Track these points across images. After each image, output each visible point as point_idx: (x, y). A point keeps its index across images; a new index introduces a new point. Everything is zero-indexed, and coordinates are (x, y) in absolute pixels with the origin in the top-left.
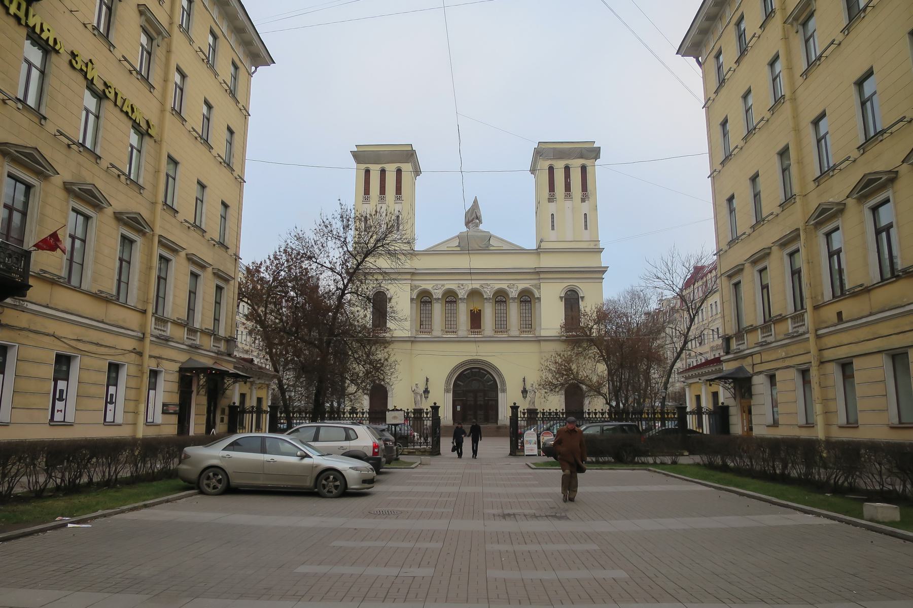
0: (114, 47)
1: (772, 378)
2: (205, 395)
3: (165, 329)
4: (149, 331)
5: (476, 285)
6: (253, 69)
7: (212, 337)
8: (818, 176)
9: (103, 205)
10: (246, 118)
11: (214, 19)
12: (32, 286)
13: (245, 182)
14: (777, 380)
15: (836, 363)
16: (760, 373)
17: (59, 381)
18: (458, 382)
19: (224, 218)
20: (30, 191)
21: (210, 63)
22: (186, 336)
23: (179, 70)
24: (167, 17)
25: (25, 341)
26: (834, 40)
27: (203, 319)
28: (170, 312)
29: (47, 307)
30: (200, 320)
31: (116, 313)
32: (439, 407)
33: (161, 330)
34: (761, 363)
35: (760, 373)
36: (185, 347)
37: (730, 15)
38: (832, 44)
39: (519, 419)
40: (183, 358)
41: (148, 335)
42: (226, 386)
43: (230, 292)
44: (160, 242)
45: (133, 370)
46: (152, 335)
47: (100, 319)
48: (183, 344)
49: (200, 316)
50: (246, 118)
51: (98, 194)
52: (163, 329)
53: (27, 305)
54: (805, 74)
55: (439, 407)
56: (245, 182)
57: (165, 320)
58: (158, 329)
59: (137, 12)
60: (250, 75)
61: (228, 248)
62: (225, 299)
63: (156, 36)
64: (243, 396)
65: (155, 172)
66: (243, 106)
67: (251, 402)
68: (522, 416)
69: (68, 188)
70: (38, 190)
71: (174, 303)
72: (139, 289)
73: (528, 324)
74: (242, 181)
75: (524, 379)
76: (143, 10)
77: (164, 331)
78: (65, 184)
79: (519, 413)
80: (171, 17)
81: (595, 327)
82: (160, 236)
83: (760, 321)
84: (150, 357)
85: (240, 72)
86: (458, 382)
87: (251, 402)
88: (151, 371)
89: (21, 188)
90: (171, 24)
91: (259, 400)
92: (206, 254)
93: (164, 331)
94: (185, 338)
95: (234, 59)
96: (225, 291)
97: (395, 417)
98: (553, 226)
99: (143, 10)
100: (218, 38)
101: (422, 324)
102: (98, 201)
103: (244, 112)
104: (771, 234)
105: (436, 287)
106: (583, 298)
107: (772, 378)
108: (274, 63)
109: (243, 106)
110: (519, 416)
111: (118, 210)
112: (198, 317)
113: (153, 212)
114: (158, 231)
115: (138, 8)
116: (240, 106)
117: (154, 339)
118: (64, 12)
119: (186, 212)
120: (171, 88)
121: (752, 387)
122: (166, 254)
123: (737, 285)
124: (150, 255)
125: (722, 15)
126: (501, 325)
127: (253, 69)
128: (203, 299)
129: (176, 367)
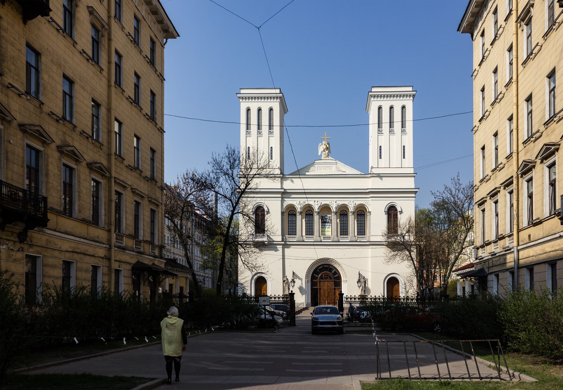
0: (77, 43)
1: (497, 276)
2: (148, 286)
3: (122, 242)
4: (113, 244)
5: (325, 202)
6: (165, 40)
7: (151, 246)
8: (526, 139)
9: (81, 160)
10: (162, 82)
11: (136, 6)
12: (50, 220)
13: (165, 132)
14: (534, 272)
15: (548, 264)
16: (492, 273)
17: (183, 321)
18: (315, 275)
19: (152, 160)
20: (39, 155)
21: (136, 41)
22: (134, 246)
23: (117, 52)
24: (106, 12)
25: (46, 254)
26: (538, 43)
27: (144, 233)
28: (124, 230)
29: (55, 230)
30: (142, 234)
31: (94, 232)
32: (294, 294)
33: (119, 243)
34: (492, 267)
35: (492, 273)
36: (134, 253)
37: (491, 6)
38: (537, 45)
39: (344, 302)
40: (134, 261)
41: (113, 247)
42: (161, 279)
43: (161, 211)
44: (115, 182)
45: (106, 270)
46: (115, 247)
47: (85, 237)
48: (133, 251)
49: (142, 232)
50: (162, 82)
51: (77, 153)
52: (121, 242)
53: (45, 231)
54: (525, 63)
55: (294, 294)
56: (165, 132)
57: (122, 235)
58: (118, 242)
59: (88, 13)
60: (163, 46)
61: (157, 182)
62: (157, 219)
63: (101, 29)
64: (171, 286)
65: (109, 132)
66: (160, 73)
67: (176, 291)
68: (346, 300)
69: (60, 149)
70: (44, 154)
71: (126, 224)
72: (105, 215)
73: (362, 231)
74: (163, 131)
75: (359, 273)
76: (91, 11)
77: (121, 243)
78: (58, 147)
79: (344, 298)
80: (109, 12)
81: (407, 234)
82: (115, 178)
83: (493, 238)
84: (115, 260)
85: (156, 45)
86: (315, 275)
87: (176, 291)
88: (116, 270)
89: (33, 153)
90: (109, 17)
91: (181, 288)
92: (143, 187)
93: (121, 243)
94: (134, 248)
95: (152, 37)
96: (157, 212)
97: (264, 301)
98: (380, 156)
99: (91, 11)
100: (140, 21)
101: (295, 224)
102: (76, 156)
103: (161, 77)
104: (502, 177)
105: (298, 203)
106: (401, 212)
107: (497, 276)
108: (179, 36)
109: (160, 73)
110: (344, 300)
111: (89, 161)
112: (141, 232)
113: (109, 160)
114: (114, 174)
115: (88, 9)
116: (158, 73)
117: (116, 249)
118: (45, 23)
119: (130, 159)
120: (113, 66)
121: (488, 282)
122: (120, 190)
123: (483, 211)
124: (110, 191)
125: (486, 4)
126: (344, 231)
127: (165, 40)
128: (143, 220)
129: (129, 267)
